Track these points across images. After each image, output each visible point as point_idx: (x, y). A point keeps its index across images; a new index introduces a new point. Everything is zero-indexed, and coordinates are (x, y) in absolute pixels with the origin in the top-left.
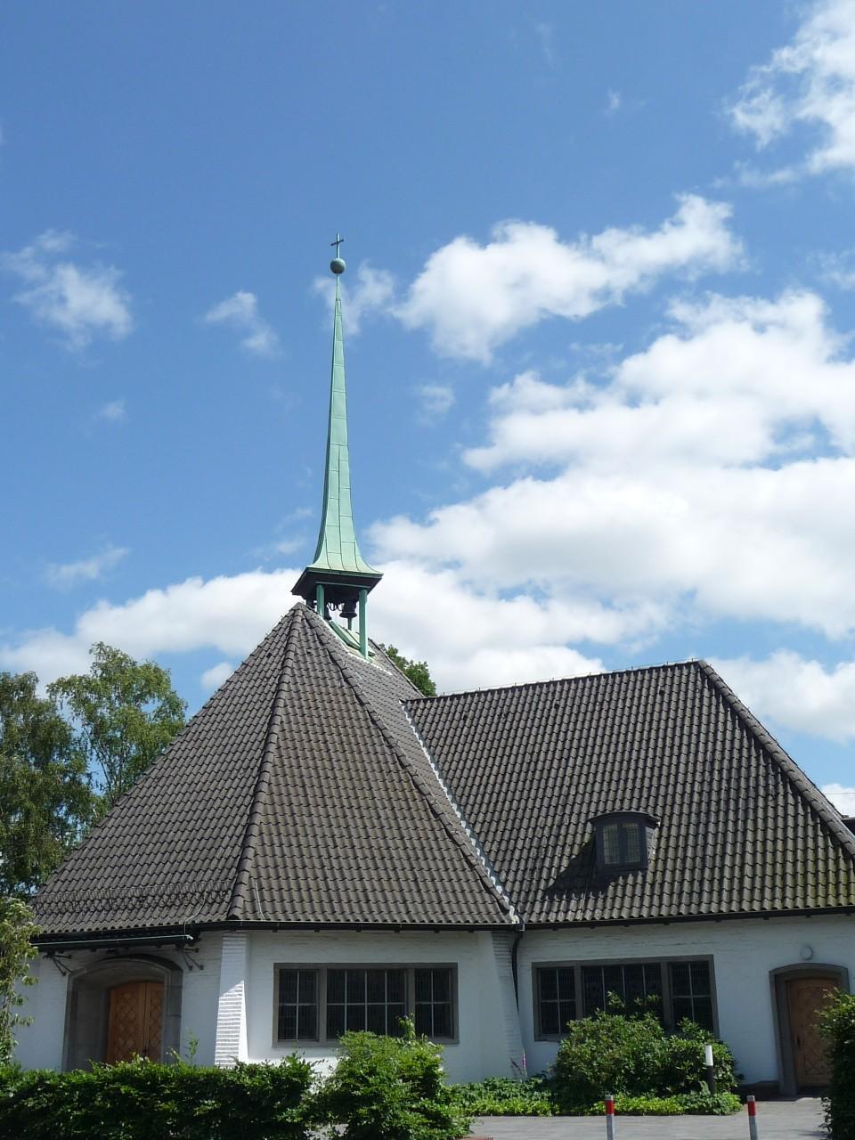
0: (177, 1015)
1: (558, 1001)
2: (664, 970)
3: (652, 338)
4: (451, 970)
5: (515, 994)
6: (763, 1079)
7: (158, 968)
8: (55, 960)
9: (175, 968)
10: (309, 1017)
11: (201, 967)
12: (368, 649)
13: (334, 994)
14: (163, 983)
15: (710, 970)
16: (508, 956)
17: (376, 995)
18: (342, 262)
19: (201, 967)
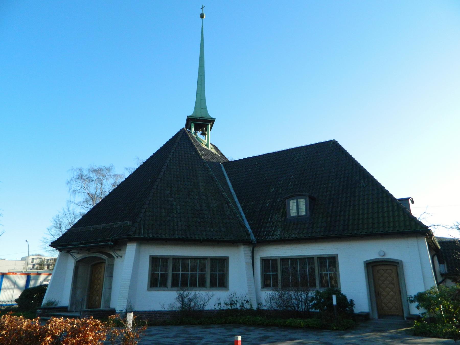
0: (111, 276)
1: (180, 273)
2: (316, 260)
3: (342, 295)
4: (226, 259)
5: (252, 270)
6: (363, 311)
7: (104, 257)
8: (71, 255)
9: (111, 256)
10: (164, 277)
11: (121, 257)
12: (210, 146)
13: (213, 269)
14: (105, 262)
15: (336, 260)
16: (250, 254)
17: (194, 269)
18: (205, 17)
19: (121, 257)
